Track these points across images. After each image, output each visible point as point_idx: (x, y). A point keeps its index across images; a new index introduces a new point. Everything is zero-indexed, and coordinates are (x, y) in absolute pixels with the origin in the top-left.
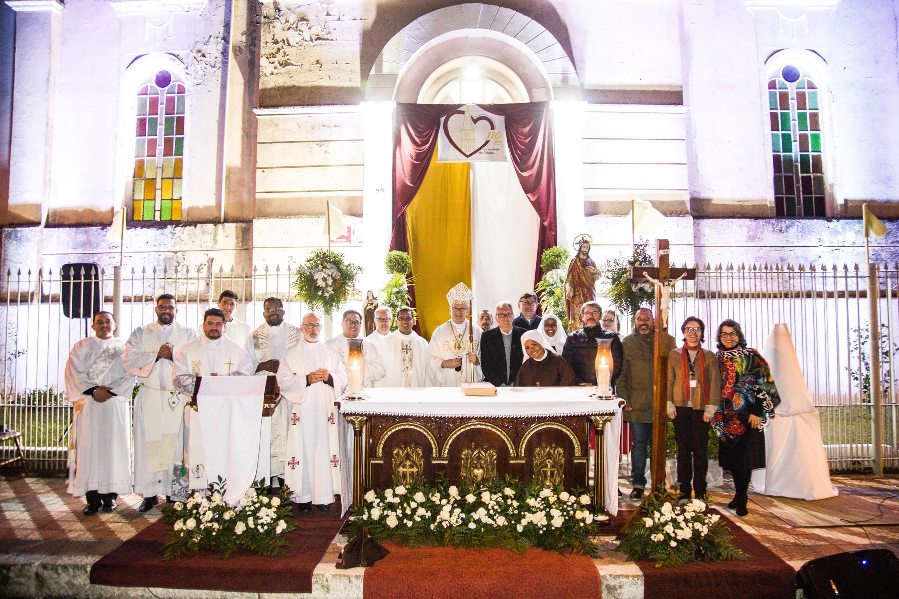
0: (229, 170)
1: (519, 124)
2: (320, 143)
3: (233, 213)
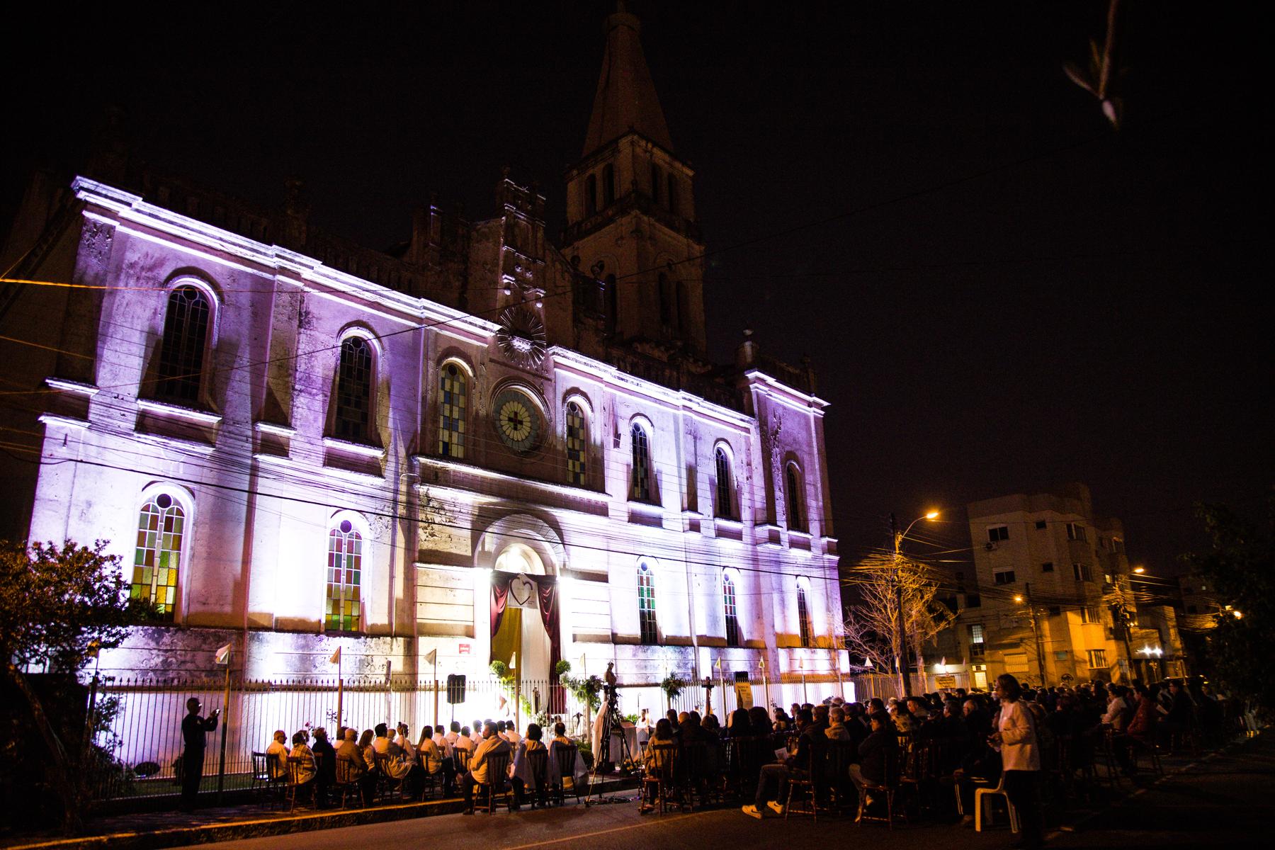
1: (543, 585)
2: (451, 589)
3: (399, 631)
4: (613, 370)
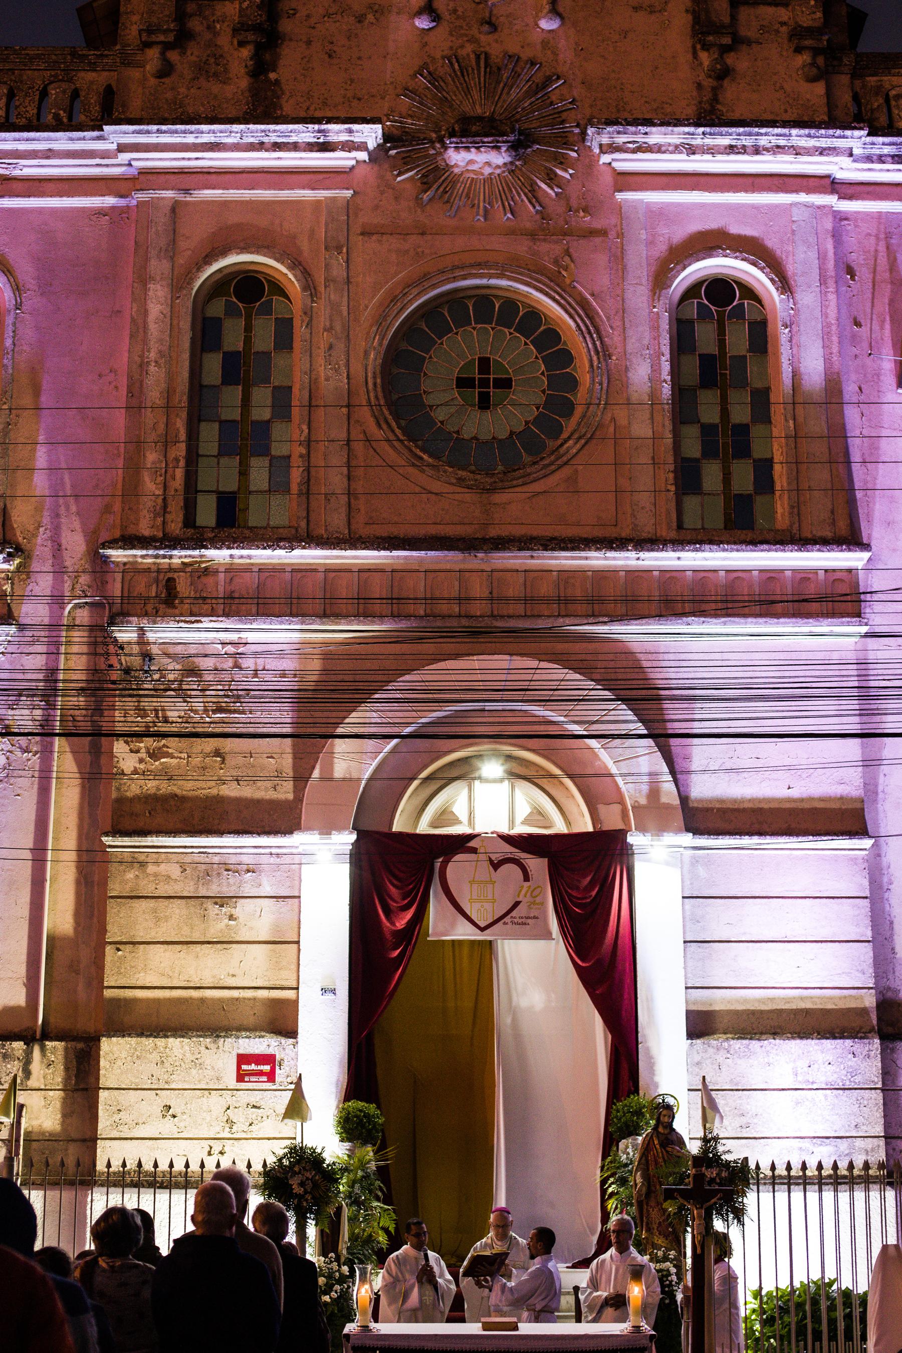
0: (52, 940)
2: (222, 901)
4: (857, 140)
